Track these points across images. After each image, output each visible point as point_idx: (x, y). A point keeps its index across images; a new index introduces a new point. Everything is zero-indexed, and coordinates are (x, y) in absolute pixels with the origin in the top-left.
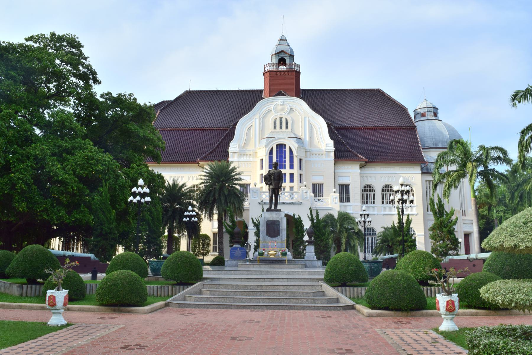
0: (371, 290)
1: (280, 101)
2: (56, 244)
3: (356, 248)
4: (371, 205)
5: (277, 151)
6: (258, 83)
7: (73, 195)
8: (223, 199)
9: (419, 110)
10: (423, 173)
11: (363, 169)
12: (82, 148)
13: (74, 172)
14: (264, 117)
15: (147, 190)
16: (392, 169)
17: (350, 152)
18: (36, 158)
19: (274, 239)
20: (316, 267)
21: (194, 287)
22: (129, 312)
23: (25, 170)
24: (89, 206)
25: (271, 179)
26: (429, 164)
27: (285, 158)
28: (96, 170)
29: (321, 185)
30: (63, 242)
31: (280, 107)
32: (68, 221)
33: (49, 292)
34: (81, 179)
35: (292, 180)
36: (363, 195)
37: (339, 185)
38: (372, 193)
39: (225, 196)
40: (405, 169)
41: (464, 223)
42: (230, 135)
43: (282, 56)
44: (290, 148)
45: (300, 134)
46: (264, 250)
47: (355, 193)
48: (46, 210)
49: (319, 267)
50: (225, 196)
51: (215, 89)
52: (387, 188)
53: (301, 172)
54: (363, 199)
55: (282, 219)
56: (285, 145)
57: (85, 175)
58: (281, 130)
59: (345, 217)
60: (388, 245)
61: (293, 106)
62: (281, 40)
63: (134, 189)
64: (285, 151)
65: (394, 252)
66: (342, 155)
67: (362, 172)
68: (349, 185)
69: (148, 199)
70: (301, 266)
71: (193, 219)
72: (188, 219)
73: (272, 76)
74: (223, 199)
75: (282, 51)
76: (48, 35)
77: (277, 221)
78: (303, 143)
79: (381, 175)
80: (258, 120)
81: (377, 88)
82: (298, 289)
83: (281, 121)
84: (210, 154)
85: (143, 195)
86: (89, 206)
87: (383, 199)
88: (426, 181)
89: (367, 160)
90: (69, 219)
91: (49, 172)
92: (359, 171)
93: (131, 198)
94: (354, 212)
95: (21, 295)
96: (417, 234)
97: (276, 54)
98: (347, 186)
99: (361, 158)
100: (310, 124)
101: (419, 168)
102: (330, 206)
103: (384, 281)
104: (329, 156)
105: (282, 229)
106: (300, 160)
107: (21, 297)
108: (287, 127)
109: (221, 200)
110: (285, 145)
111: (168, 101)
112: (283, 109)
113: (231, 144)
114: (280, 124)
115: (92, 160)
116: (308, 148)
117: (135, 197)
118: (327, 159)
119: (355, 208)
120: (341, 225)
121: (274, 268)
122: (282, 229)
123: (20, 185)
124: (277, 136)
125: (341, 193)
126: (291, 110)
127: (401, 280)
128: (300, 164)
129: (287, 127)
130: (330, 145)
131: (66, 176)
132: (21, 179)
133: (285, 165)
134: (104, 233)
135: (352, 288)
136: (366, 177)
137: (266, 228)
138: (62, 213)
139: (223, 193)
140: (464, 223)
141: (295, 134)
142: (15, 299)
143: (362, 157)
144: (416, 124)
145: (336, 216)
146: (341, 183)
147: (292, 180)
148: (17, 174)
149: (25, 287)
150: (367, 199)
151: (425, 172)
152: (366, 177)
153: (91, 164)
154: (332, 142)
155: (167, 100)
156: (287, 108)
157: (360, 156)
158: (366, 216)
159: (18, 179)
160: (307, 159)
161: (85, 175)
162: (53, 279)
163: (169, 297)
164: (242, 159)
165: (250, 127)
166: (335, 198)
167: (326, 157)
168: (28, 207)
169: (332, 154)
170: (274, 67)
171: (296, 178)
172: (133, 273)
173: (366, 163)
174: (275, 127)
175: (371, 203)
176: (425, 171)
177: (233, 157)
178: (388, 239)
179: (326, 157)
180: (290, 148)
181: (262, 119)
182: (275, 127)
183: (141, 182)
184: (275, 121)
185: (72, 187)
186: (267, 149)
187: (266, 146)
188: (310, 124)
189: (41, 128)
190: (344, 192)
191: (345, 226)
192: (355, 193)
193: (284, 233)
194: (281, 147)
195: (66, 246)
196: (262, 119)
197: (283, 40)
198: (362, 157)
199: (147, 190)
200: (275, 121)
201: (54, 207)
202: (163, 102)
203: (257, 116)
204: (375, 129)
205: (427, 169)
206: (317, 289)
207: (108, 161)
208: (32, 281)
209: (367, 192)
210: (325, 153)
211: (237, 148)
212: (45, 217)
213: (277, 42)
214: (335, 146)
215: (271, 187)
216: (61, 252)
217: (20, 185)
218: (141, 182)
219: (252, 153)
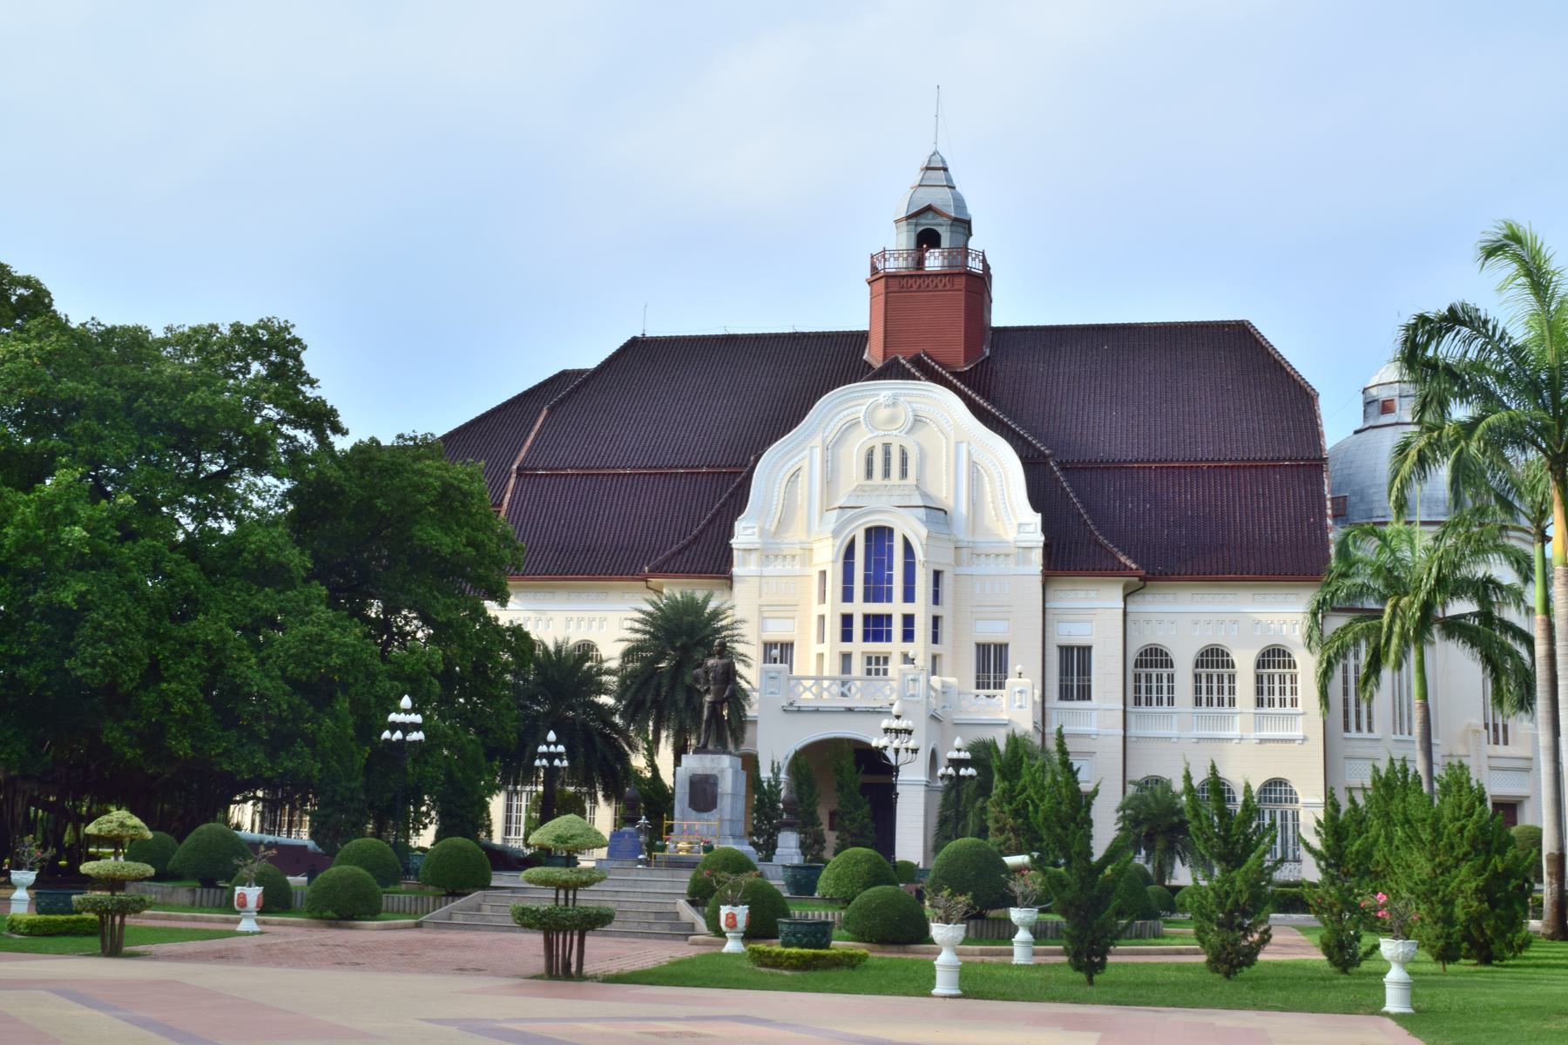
1: (884, 393)
2: (244, 815)
6: (849, 309)
7: (281, 720)
9: (1374, 392)
12: (303, 615)
13: (284, 670)
14: (839, 440)
16: (1230, 598)
18: (207, 645)
19: (705, 815)
22: (351, 928)
23: (189, 676)
24: (311, 742)
27: (890, 568)
28: (328, 666)
29: (1002, 649)
30: (262, 814)
31: (883, 414)
32: (268, 774)
33: (238, 889)
34: (296, 685)
35: (908, 636)
38: (1165, 672)
40: (1269, 598)
41: (1492, 768)
42: (733, 494)
43: (927, 222)
45: (943, 491)
47: (1107, 674)
48: (227, 753)
51: (721, 332)
52: (1213, 658)
53: (938, 611)
55: (722, 771)
56: (891, 530)
57: (304, 678)
58: (886, 482)
61: (925, 409)
62: (928, 168)
63: (393, 717)
64: (891, 548)
66: (1066, 556)
69: (418, 736)
71: (557, 762)
72: (545, 762)
73: (894, 288)
75: (929, 209)
76: (226, 331)
79: (1188, 618)
80: (818, 453)
81: (1239, 318)
83: (887, 453)
85: (406, 728)
86: (311, 742)
87: (1198, 690)
89: (1142, 572)
90: (272, 769)
91: (234, 676)
93: (386, 734)
94: (1102, 731)
95: (193, 904)
96: (1301, 800)
97: (908, 218)
98: (1085, 651)
100: (973, 466)
104: (1028, 561)
106: (937, 575)
107: (192, 906)
108: (904, 474)
110: (891, 530)
111: (579, 372)
112: (892, 420)
113: (739, 525)
114: (885, 462)
115: (320, 643)
116: (964, 537)
117: (393, 732)
118: (1021, 569)
123: (180, 706)
124: (870, 502)
125: (1065, 670)
126: (918, 420)
129: (904, 474)
130: (1031, 529)
131: (267, 683)
132: (181, 695)
133: (890, 590)
134: (338, 798)
138: (259, 757)
139: (688, 675)
140: (1492, 768)
141: (924, 495)
142: (183, 908)
147: (908, 636)
148: (173, 685)
149: (199, 891)
150: (1149, 690)
153: (317, 652)
154: (1037, 518)
155: (576, 367)
156: (905, 415)
159: (177, 693)
160: (960, 570)
161: (304, 678)
162: (244, 872)
163: (423, 914)
164: (770, 570)
165: (795, 474)
166: (1021, 692)
167: (1017, 564)
168: (193, 747)
169: (1037, 557)
170: (902, 263)
171: (922, 628)
172: (361, 871)
174: (869, 474)
175: (1210, 703)
177: (744, 563)
179: (1017, 564)
181: (831, 451)
182: (869, 474)
184: (870, 453)
185: (279, 705)
186: (838, 542)
187: (835, 534)
188: (973, 466)
190: (1073, 673)
192: (1107, 674)
194: (879, 537)
195: (270, 819)
196: (831, 451)
197: (936, 168)
198: (1128, 563)
200: (870, 453)
201: (243, 746)
202: (564, 376)
203: (817, 441)
204: (1191, 469)
206: (669, 908)
207: (354, 646)
208: (208, 883)
209: (1149, 670)
210: (1013, 551)
211: (756, 538)
212: (226, 767)
213: (917, 177)
214: (1046, 528)
216: (257, 835)
217: (180, 706)
219: (799, 552)
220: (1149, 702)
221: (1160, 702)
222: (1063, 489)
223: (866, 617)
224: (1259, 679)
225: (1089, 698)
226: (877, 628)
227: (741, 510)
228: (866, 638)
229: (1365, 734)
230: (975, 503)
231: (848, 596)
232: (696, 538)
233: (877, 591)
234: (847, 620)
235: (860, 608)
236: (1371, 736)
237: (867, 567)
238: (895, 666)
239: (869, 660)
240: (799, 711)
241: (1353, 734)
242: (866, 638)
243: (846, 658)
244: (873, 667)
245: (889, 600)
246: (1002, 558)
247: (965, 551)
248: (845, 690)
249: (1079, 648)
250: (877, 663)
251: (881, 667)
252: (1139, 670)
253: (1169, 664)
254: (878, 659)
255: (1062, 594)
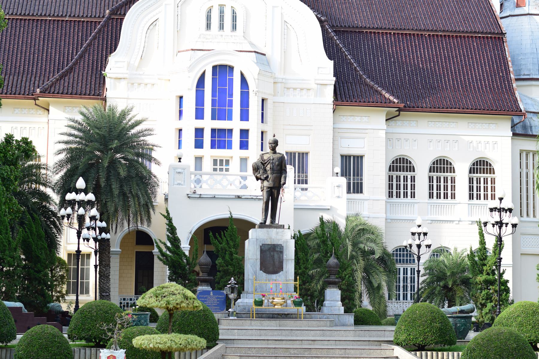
0: (471, 352)
3: (381, 292)
4: (405, 200)
5: (214, 80)
8: (115, 187)
10: (515, 134)
11: (391, 122)
15: (91, 197)
17: (367, 85)
20: (347, 325)
21: (215, 351)
25: (265, 171)
26: (528, 115)
27: (231, 95)
36: (390, 178)
37: (342, 156)
38: (409, 174)
39: (122, 182)
44: (242, 75)
46: (264, 296)
47: (375, 175)
49: (350, 326)
50: (122, 182)
52: (441, 165)
53: (264, 127)
54: (390, 186)
56: (231, 68)
59: (362, 231)
60: (445, 287)
64: (231, 81)
65: (458, 301)
66: (348, 91)
67: (391, 130)
68: (362, 157)
70: (328, 323)
74: (115, 187)
77: (278, 245)
78: (268, 64)
79: (429, 137)
82: (362, 354)
83: (222, 12)
84: (62, 77)
87: (431, 187)
88: (521, 152)
92: (385, 127)
99: (390, 102)
101: (509, 125)
102: (325, 204)
103: (488, 340)
105: (287, 260)
108: (234, 27)
109: (111, 189)
110: (231, 68)
116: (279, 75)
119: (373, 207)
120: (355, 245)
121: (286, 326)
122: (287, 260)
127: (509, 340)
128: (263, 110)
129: (234, 27)
133: (230, 112)
135: (434, 353)
136: (399, 140)
137: (259, 257)
141: (251, 44)
143: (391, 98)
144: (503, 23)
145: (342, 225)
146: (346, 152)
147: (244, 145)
150: (398, 187)
151: (521, 132)
152: (399, 140)
154: (331, 64)
157: (387, 95)
158: (422, 235)
166: (338, 186)
169: (330, 90)
173: (400, 110)
174: (208, 26)
176: (519, 131)
178: (445, 274)
180: (242, 75)
182: (208, 26)
183: (81, 183)
184: (209, 11)
189: (99, 151)
190: (351, 168)
191: (362, 246)
192: (375, 175)
193: (290, 267)
194: (222, 71)
198: (391, 98)
199: (91, 197)
205: (525, 127)
209: (398, 173)
215: (266, 183)
218: (81, 183)
220: (398, 195)
221: (406, 195)
222: (337, 45)
223: (213, 131)
224: (471, 180)
225: (361, 192)
226: (221, 138)
227: (113, 46)
228: (213, 146)
229: (531, 218)
230: (285, 52)
231: (199, 115)
232: (71, 68)
233: (221, 112)
234: (199, 132)
235: (208, 124)
236: (535, 220)
237: (213, 95)
238: (235, 166)
239: (215, 161)
240: (200, 197)
241: (525, 218)
242: (213, 146)
243: (199, 160)
244: (218, 167)
245: (230, 118)
246: (304, 92)
247: (279, 85)
248: (243, 182)
249: (354, 157)
250: (221, 164)
251: (224, 167)
252: (392, 173)
253: (412, 169)
254: (221, 161)
255: (344, 118)
